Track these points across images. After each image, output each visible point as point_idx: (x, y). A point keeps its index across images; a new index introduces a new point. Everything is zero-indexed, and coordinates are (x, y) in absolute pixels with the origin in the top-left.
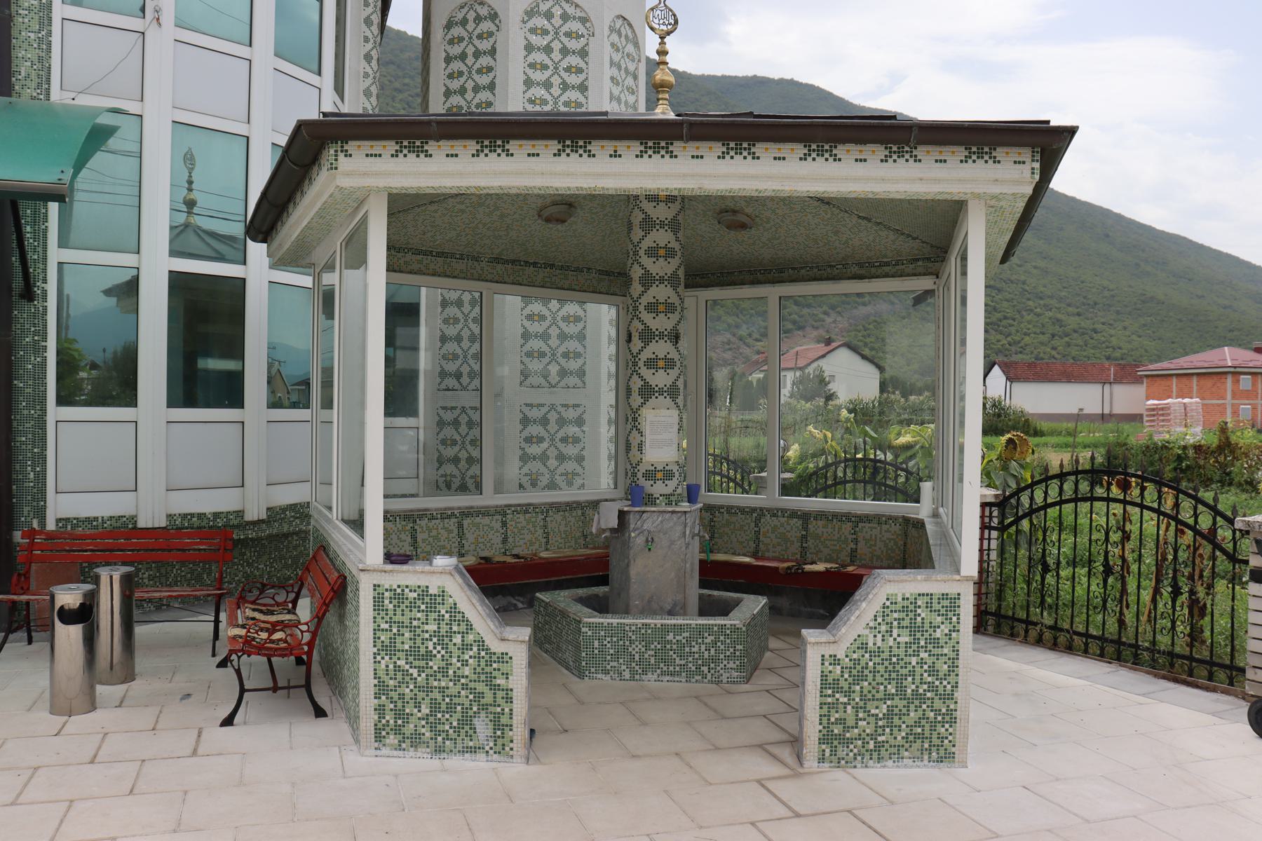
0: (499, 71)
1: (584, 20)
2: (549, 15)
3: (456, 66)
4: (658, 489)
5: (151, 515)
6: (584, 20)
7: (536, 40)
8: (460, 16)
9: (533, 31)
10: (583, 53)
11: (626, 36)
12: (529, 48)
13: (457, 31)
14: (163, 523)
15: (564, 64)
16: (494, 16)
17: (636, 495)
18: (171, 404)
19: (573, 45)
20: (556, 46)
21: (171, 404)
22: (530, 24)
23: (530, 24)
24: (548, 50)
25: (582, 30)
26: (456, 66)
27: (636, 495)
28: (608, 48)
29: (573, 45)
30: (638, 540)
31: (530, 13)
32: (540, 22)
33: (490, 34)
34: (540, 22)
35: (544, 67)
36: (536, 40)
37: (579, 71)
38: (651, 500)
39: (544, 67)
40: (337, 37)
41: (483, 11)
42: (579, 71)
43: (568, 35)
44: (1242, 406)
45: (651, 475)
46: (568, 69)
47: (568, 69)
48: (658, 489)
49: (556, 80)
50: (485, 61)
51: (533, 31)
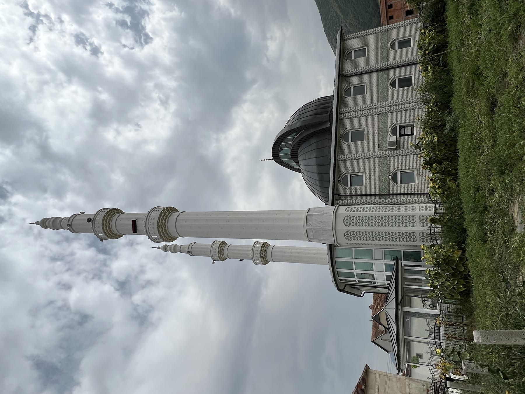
2: (347, 222)
8: (347, 238)
10: (353, 217)
19: (352, 218)
31: (347, 226)
41: (346, 234)
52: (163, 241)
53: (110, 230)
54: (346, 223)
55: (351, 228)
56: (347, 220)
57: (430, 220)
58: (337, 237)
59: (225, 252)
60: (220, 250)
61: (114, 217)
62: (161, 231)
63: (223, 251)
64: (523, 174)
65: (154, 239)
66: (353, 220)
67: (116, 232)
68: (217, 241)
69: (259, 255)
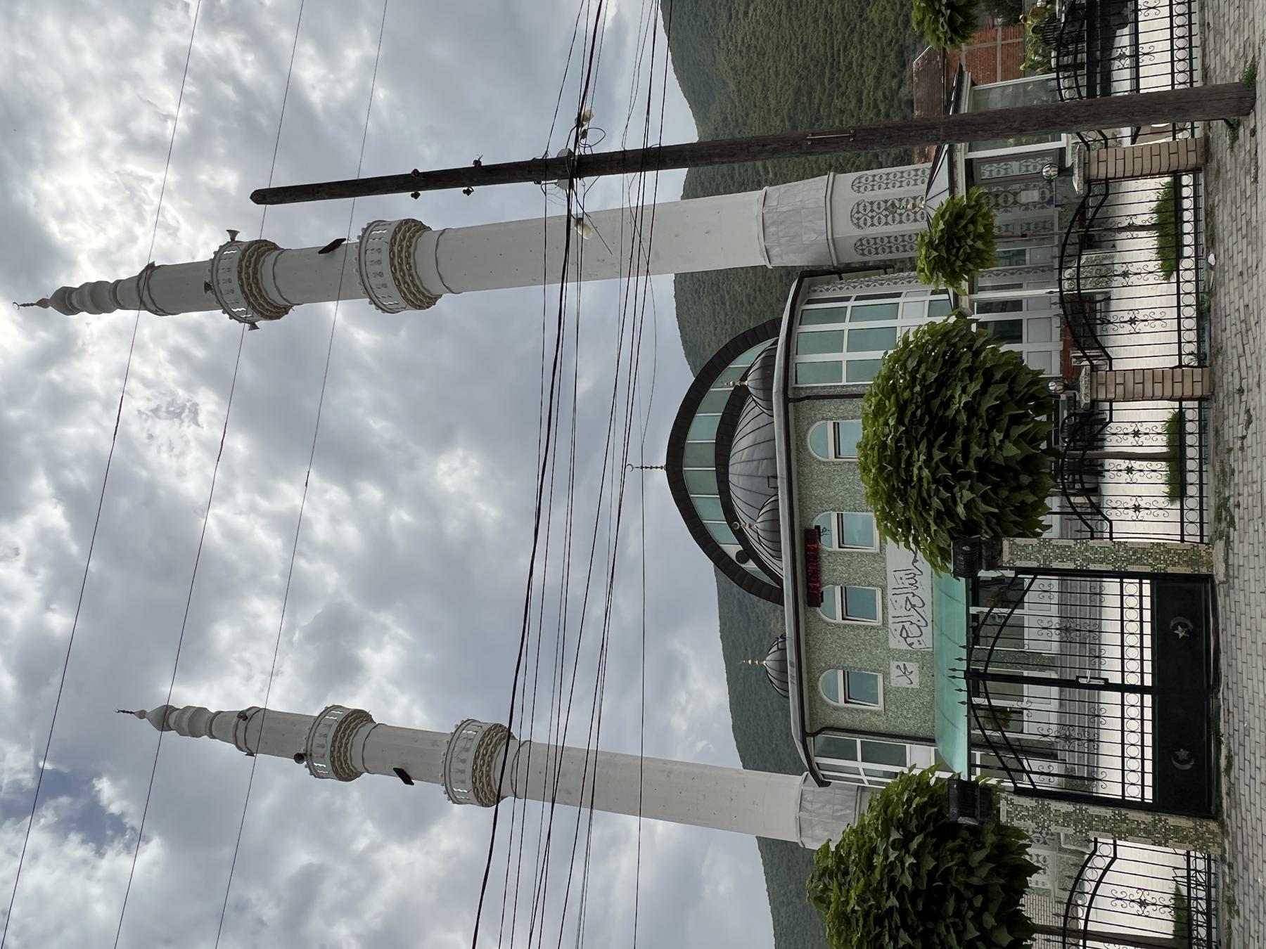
0: (909, 233)
1: (858, 204)
2: (858, 219)
3: (894, 249)
4: (1048, 195)
5: (1060, 346)
6: (858, 204)
7: (869, 223)
8: (861, 252)
9: (865, 224)
10: (872, 203)
11: (859, 183)
12: (873, 225)
13: (866, 252)
14: (1062, 343)
15: (877, 210)
16: (861, 240)
17: (1050, 201)
18: (1021, 342)
19: (869, 208)
20: (870, 214)
21: (1021, 342)
22: (863, 226)
23: (863, 226)
24: (872, 217)
25: (863, 204)
26: (894, 249)
27: (1050, 201)
28: (866, 193)
29: (869, 208)
30: (1065, 201)
31: (859, 226)
32: (861, 222)
33: (868, 240)
34: (861, 222)
35: (879, 218)
36: (869, 223)
37: (879, 204)
38: (1052, 197)
39: (879, 218)
40: (789, 352)
41: (859, 243)
42: (879, 204)
43: (865, 210)
44: (879, 593)
45: (1043, 198)
46: (879, 208)
47: (879, 208)
48: (1048, 195)
49: (860, 215)
50: (878, 241)
51: (865, 224)
52: (334, 776)
53: (268, 303)
54: (856, 221)
55: (869, 231)
56: (858, 212)
57: (1033, 31)
58: (834, 191)
59: (356, 751)
60: (344, 732)
61: (415, 250)
62: (405, 290)
63: (349, 762)
64: (951, 923)
65: (316, 771)
66: (872, 211)
67: (274, 296)
68: (474, 721)
69: (386, 248)
